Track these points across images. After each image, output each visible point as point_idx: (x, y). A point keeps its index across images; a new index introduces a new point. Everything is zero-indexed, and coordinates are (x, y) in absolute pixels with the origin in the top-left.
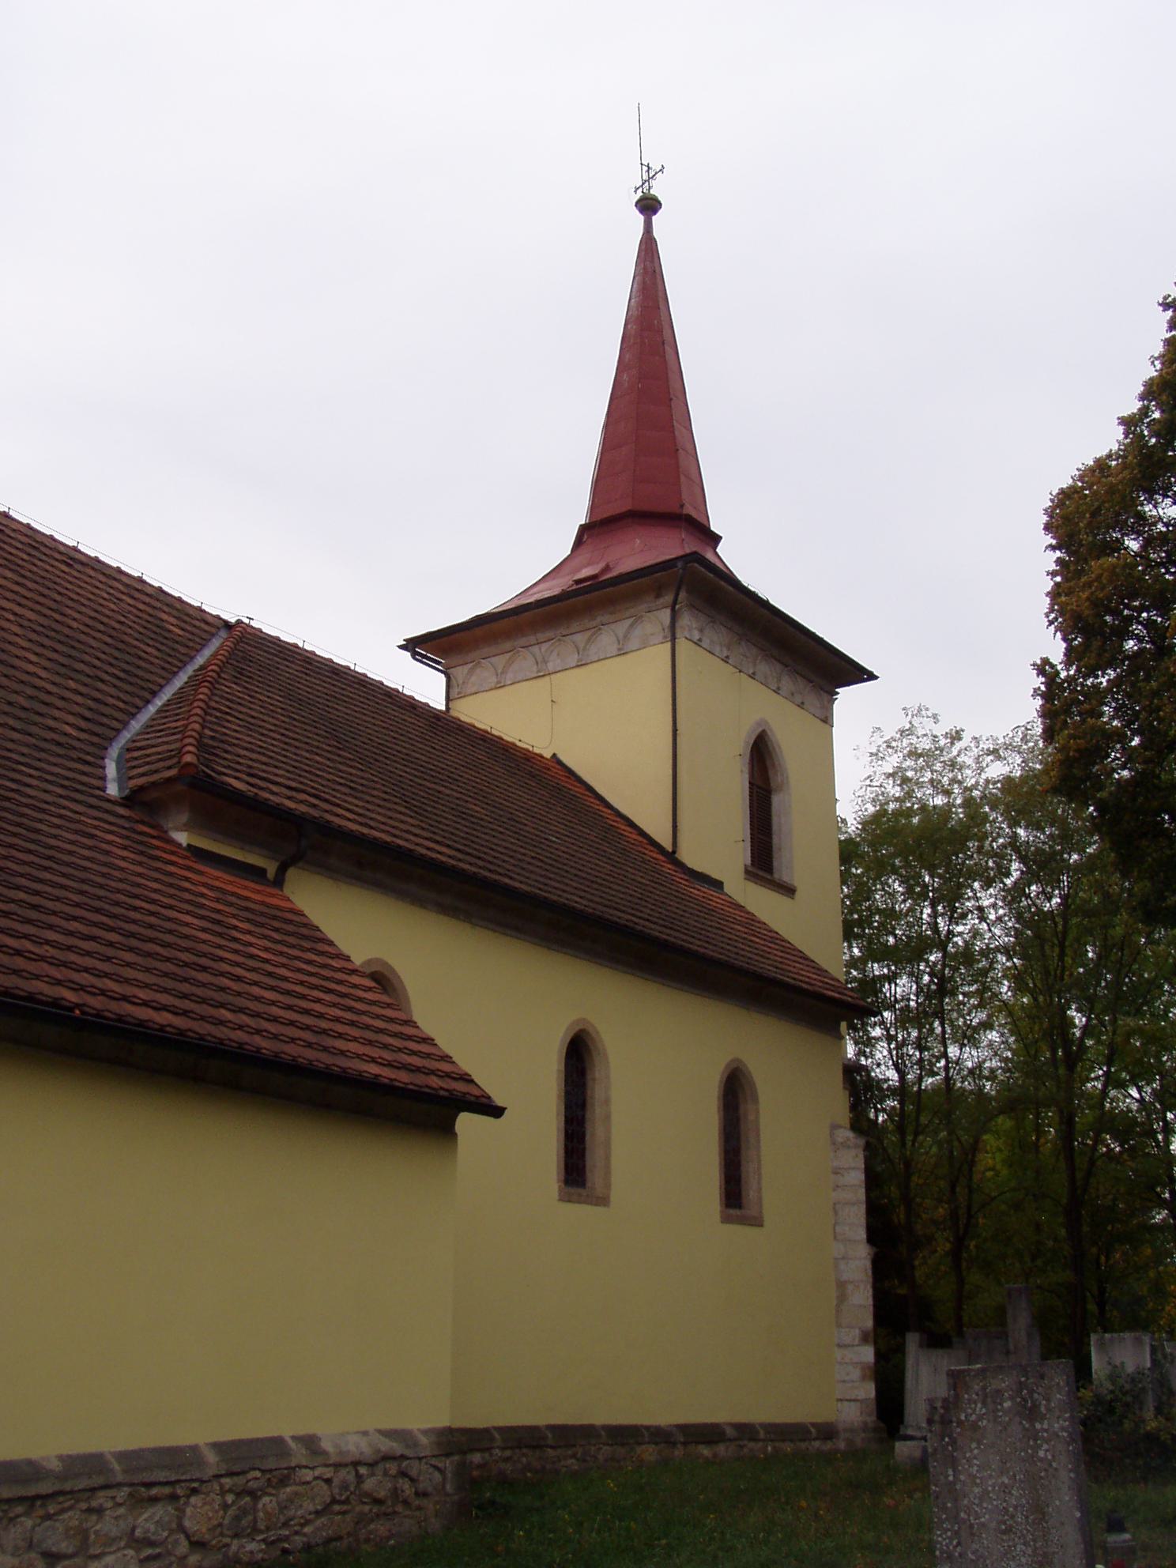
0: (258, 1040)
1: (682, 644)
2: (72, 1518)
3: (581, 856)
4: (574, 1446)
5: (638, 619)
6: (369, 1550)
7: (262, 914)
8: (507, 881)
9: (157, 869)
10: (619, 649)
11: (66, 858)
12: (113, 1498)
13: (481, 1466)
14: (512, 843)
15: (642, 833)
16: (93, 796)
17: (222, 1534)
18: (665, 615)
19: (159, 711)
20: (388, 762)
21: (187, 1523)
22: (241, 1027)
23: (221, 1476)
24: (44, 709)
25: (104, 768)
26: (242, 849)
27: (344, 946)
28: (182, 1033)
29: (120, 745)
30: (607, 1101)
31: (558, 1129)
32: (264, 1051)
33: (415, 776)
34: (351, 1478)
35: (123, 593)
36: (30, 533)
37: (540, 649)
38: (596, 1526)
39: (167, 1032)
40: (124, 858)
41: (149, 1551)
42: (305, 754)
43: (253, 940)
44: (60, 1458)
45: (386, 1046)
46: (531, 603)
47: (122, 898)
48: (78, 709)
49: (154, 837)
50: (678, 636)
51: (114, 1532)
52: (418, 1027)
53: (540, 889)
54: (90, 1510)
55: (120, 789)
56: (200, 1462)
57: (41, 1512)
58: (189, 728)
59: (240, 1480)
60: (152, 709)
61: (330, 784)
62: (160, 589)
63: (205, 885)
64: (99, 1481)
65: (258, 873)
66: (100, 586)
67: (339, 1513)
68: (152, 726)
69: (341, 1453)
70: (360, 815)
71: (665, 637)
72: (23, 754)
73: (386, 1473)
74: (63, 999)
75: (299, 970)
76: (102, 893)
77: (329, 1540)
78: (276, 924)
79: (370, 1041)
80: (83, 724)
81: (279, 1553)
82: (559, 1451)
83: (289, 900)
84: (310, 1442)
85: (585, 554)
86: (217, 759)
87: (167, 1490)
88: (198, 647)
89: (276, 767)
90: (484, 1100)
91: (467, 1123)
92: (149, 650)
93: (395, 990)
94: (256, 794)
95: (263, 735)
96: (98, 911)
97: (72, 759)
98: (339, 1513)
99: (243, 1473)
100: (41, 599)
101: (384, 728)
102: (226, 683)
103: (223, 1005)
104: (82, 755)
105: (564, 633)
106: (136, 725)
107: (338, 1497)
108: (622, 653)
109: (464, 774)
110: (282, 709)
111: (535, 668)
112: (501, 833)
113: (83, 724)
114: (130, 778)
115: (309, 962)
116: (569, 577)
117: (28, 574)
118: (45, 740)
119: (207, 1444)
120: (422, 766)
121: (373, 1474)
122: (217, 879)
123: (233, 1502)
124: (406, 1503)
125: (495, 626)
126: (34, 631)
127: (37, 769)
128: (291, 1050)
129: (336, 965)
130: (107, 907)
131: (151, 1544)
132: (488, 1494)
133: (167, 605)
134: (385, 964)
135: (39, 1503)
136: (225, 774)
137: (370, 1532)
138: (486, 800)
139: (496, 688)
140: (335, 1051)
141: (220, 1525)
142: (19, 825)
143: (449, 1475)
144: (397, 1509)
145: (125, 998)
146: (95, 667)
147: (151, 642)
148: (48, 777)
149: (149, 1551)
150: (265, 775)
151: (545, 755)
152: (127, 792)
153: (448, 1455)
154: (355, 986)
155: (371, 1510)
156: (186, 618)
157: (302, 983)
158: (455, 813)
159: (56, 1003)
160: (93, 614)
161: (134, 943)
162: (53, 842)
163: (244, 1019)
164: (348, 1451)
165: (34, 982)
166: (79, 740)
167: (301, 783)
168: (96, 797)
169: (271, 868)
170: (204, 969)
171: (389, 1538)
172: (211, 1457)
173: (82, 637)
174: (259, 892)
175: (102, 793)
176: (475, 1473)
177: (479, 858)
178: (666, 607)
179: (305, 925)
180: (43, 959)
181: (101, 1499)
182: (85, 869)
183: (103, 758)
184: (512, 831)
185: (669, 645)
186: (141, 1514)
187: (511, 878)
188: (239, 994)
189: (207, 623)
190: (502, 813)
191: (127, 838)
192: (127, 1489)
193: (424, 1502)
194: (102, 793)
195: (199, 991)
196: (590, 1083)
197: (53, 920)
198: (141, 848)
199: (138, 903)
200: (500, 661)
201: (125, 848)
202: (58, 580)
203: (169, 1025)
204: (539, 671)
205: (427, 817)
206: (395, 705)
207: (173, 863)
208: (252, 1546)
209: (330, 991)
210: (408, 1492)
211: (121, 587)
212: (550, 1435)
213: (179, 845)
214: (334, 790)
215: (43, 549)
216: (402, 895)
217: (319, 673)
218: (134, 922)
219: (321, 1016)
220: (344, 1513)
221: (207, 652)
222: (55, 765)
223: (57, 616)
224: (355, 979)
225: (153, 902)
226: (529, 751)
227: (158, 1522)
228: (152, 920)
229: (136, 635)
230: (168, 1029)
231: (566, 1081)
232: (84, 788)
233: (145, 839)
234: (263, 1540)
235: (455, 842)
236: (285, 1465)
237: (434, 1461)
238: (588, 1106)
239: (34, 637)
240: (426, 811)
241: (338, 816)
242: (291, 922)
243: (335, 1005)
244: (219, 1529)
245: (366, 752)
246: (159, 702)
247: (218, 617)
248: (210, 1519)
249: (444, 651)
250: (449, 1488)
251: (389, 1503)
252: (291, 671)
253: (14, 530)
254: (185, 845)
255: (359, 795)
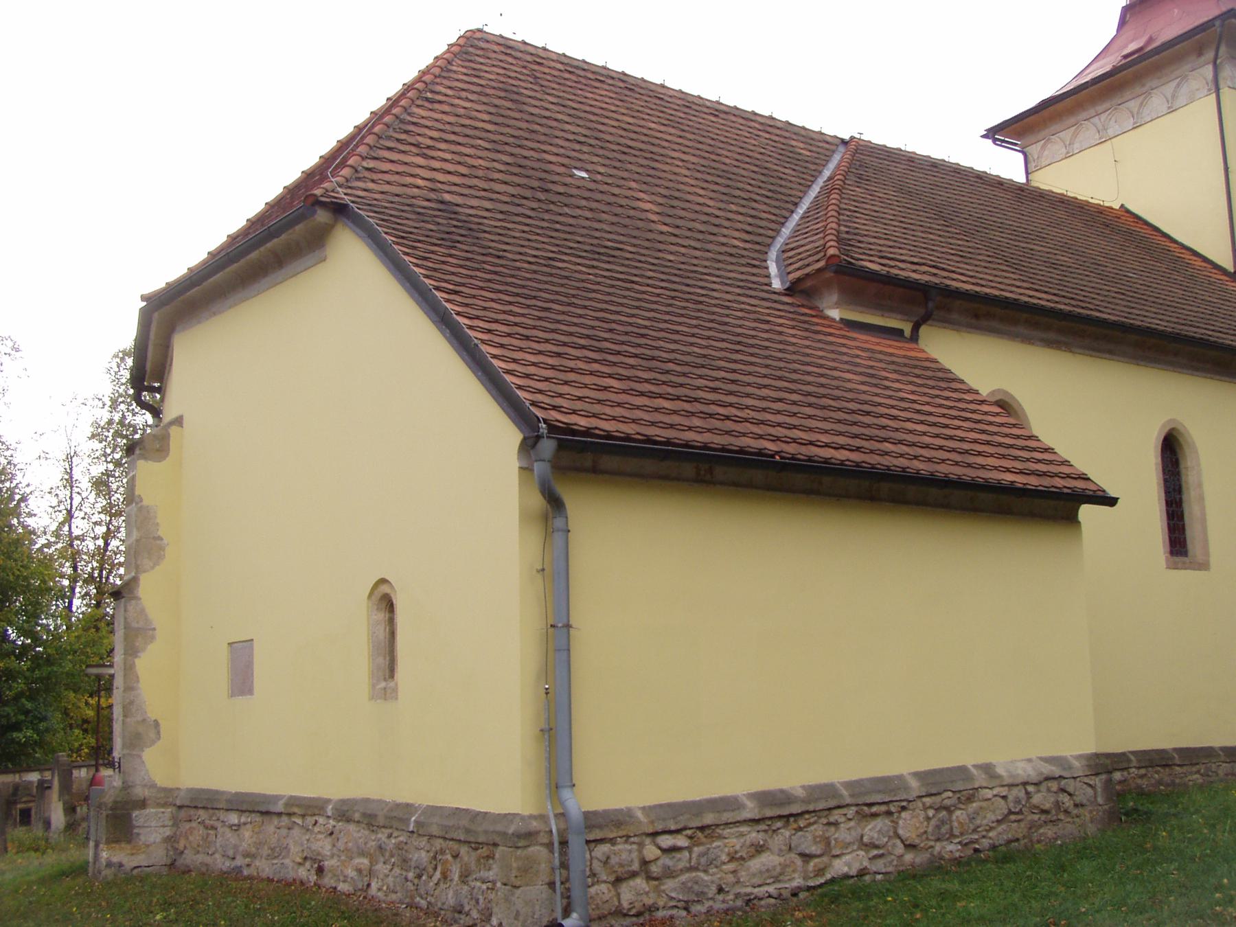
0: (917, 465)
1: (1226, 93)
2: (817, 829)
3: (1156, 286)
4: (1197, 764)
5: (1184, 78)
6: (1042, 848)
7: (905, 365)
8: (1098, 314)
9: (819, 341)
10: (1169, 108)
11: (751, 341)
12: (845, 815)
13: (1120, 782)
14: (1097, 283)
15: (1205, 259)
16: (763, 291)
17: (927, 839)
18: (1208, 71)
19: (802, 218)
20: (987, 231)
21: (901, 832)
22: (902, 456)
23: (923, 796)
24: (715, 230)
25: (767, 268)
26: (883, 316)
27: (974, 384)
28: (858, 465)
29: (776, 249)
30: (1200, 485)
31: (1160, 511)
32: (922, 472)
33: (1011, 239)
34: (1022, 794)
35: (760, 130)
36: (701, 102)
37: (1100, 119)
38: (1227, 828)
39: (846, 465)
40: (794, 336)
41: (875, 852)
42: (920, 234)
43: (901, 386)
44: (803, 787)
45: (1016, 458)
46: (1087, 82)
47: (797, 366)
48: (739, 226)
49: (813, 316)
50: (1221, 86)
51: (849, 839)
52: (1039, 440)
53: (1126, 317)
54: (829, 824)
55: (783, 283)
56: (907, 788)
57: (795, 826)
58: (828, 227)
59: (937, 799)
60: (796, 217)
61: (943, 255)
62: (788, 123)
63: (857, 348)
64: (832, 803)
65: (898, 333)
66: (741, 127)
67: (1015, 821)
68: (798, 231)
69: (1011, 776)
70: (972, 277)
71: (1209, 90)
72: (706, 267)
73: (1049, 790)
74: (765, 449)
75: (940, 406)
76: (782, 364)
77: (1009, 842)
78: (917, 371)
79: (527, 337)
80: (747, 237)
81: (972, 852)
82: (1185, 768)
83: (923, 351)
84: (987, 769)
85: (1129, 32)
86: (854, 249)
87: (883, 808)
88: (824, 163)
89: (900, 248)
90: (1100, 493)
91: (1086, 512)
92: (786, 171)
93: (1016, 412)
94: (888, 272)
95: (886, 224)
96: (780, 378)
97: (743, 265)
98: (1015, 821)
99: (939, 794)
100: (700, 146)
101: (979, 204)
102: (850, 188)
103: (885, 440)
104: (750, 261)
105: (1119, 102)
106: (786, 231)
107: (1013, 810)
108: (1172, 110)
109: (1049, 232)
110: (898, 201)
111: (1097, 136)
112: (1087, 276)
113: (747, 237)
114: (789, 273)
115: (947, 398)
116: (1117, 54)
117: (687, 128)
118: (720, 253)
119: (909, 774)
120: (1015, 231)
121: (1039, 791)
122: (866, 342)
123: (934, 816)
124: (1066, 812)
125: (1060, 106)
126: (698, 171)
127: (718, 276)
128: (943, 469)
129: (968, 398)
130: (787, 375)
131: (877, 847)
132: (1131, 804)
133: (795, 134)
134: (1006, 393)
135: (792, 819)
136: (862, 260)
137: (1041, 835)
138: (1071, 251)
139: (1066, 158)
140: (977, 466)
141: (925, 832)
142: (712, 321)
143: (1099, 790)
144: (1059, 817)
145: (811, 443)
146: (748, 191)
147: (787, 165)
148: (728, 282)
149: (875, 852)
150: (892, 256)
151: (1114, 207)
152: (788, 285)
153: (1097, 774)
154: (986, 413)
155: (1039, 819)
156: (812, 142)
157: (944, 415)
158: (1047, 265)
159: (760, 453)
160: (740, 151)
161: (813, 400)
162: (739, 330)
163: (905, 449)
164: (1018, 775)
165: (742, 438)
166: (745, 249)
167: (922, 258)
168: (767, 292)
169: (907, 328)
170: (868, 413)
171: (1056, 839)
172: (914, 783)
173: (735, 170)
174: (901, 348)
175: (769, 288)
176: (1118, 787)
177: (1072, 299)
178: (1208, 63)
179: (940, 370)
180: (746, 420)
181: (836, 816)
182: (767, 348)
183: (766, 261)
184: (1095, 273)
185: (1214, 96)
186: (866, 826)
187: (1100, 311)
188: (897, 430)
189: (827, 143)
190: (1085, 259)
191: (793, 319)
192: (854, 809)
193: (1081, 810)
194: (769, 288)
195: (867, 431)
196: (1183, 471)
197: (749, 390)
198: (806, 326)
199: (810, 369)
200: (1066, 135)
201: (793, 328)
202: (710, 129)
203: (848, 460)
204: (1100, 138)
205: (1025, 271)
206: (987, 185)
207: (830, 334)
208: (951, 847)
209: (967, 419)
210: (1067, 804)
211: (757, 126)
212: (1176, 756)
213: (833, 320)
214: (948, 260)
215: (694, 107)
216: (1013, 336)
217: (922, 169)
218: (809, 383)
219: (962, 440)
220: (1019, 821)
221: (832, 166)
222: (731, 271)
223: (713, 157)
224: (985, 408)
225: (821, 366)
226: (1100, 205)
227: (879, 831)
228: (822, 380)
229: (775, 161)
230: (847, 463)
231: (1164, 470)
232: (755, 286)
233: (807, 319)
234: (960, 843)
235: (1050, 288)
236: (971, 787)
237: (1086, 780)
238: (1184, 489)
239: (699, 175)
240: (1024, 266)
241: (954, 280)
242: (928, 368)
243: (972, 430)
244: (925, 836)
245: (969, 226)
246: (800, 211)
247: (836, 137)
248: (918, 828)
249: (1019, 135)
250: (1100, 800)
251: (1054, 812)
252: (899, 170)
253: (671, 96)
254: (838, 319)
255: (968, 261)
